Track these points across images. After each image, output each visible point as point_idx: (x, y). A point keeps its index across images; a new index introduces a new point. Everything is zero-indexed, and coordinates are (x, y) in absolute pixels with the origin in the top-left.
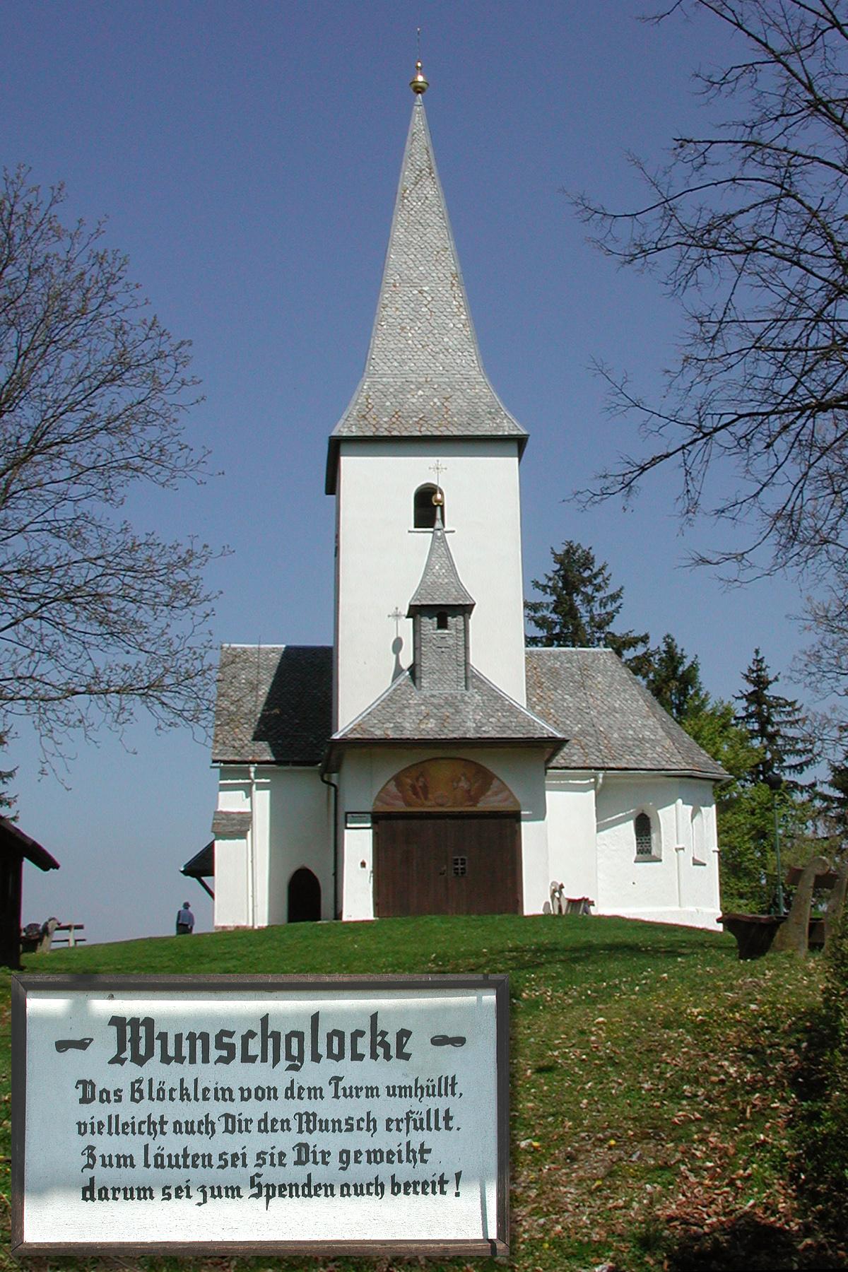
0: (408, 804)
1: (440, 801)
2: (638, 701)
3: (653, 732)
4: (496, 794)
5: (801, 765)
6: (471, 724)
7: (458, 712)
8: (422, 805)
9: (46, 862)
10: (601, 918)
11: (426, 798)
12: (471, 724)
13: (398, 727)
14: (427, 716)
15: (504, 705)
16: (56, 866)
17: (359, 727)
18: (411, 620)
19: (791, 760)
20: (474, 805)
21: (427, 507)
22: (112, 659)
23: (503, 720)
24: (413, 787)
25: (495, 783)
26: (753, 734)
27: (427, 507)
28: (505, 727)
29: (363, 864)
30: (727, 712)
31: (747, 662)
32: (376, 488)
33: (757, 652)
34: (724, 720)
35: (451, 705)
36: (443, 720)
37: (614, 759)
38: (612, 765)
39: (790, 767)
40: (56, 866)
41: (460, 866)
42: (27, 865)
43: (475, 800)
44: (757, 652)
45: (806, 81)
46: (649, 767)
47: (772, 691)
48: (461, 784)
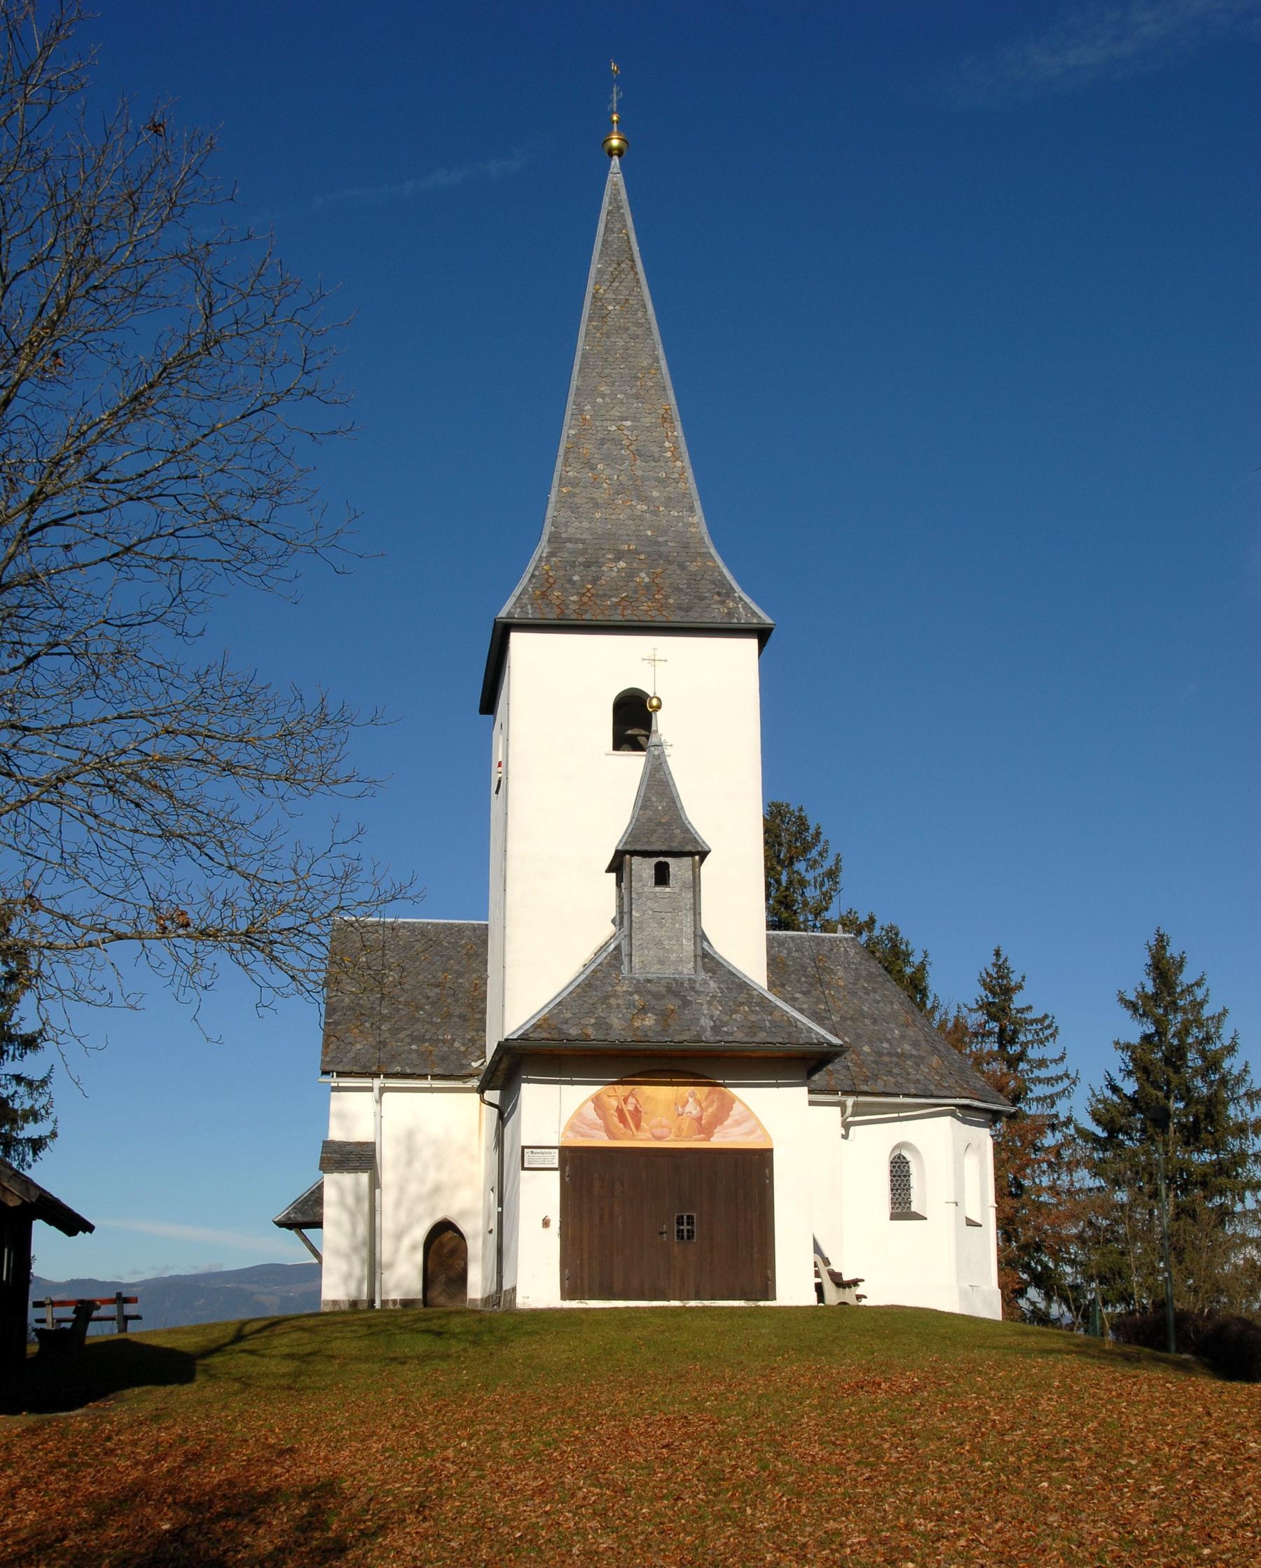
0: (612, 1135)
1: (658, 1132)
2: (892, 1003)
3: (915, 1044)
4: (738, 1123)
5: (1051, 1096)
6: (706, 1023)
7: (686, 1003)
8: (633, 1138)
9: (72, 1224)
10: (520, 1310)
11: (638, 1127)
12: (706, 1023)
13: (601, 1024)
14: (643, 1010)
15: (752, 997)
16: (88, 1228)
17: (544, 1022)
18: (613, 875)
19: (1039, 1090)
20: (707, 1139)
21: (633, 718)
22: (193, 883)
23: (752, 1018)
24: (620, 1111)
25: (736, 1107)
26: (992, 1057)
27: (633, 718)
28: (753, 1028)
29: (546, 1223)
30: (959, 1026)
31: (987, 962)
32: (559, 683)
33: (997, 954)
34: (958, 1034)
35: (676, 994)
36: (665, 1017)
37: (866, 1081)
38: (865, 1088)
39: (1038, 1099)
40: (88, 1228)
41: (685, 1227)
42: (40, 1229)
43: (708, 1132)
44: (997, 954)
45: (67, 522)
46: (913, 1091)
47: (1018, 1001)
48: (688, 1109)
